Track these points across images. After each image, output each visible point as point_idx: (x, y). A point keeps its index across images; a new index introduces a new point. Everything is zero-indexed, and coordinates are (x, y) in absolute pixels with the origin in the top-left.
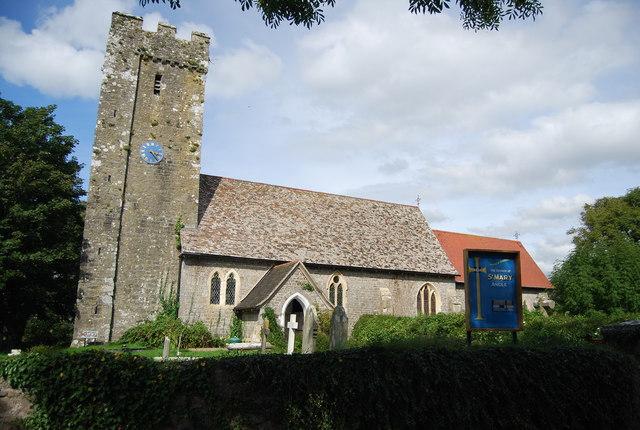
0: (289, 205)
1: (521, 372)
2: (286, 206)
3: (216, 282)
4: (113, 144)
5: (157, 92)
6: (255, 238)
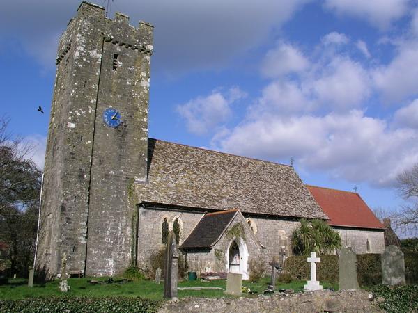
3: (165, 225)
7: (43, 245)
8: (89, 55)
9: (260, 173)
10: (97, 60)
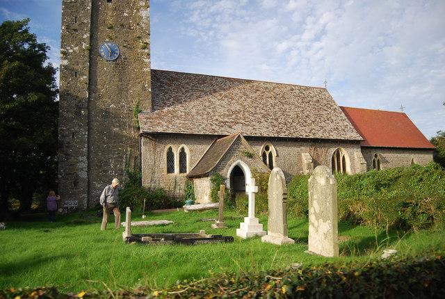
6: (199, 117)
9: (286, 96)
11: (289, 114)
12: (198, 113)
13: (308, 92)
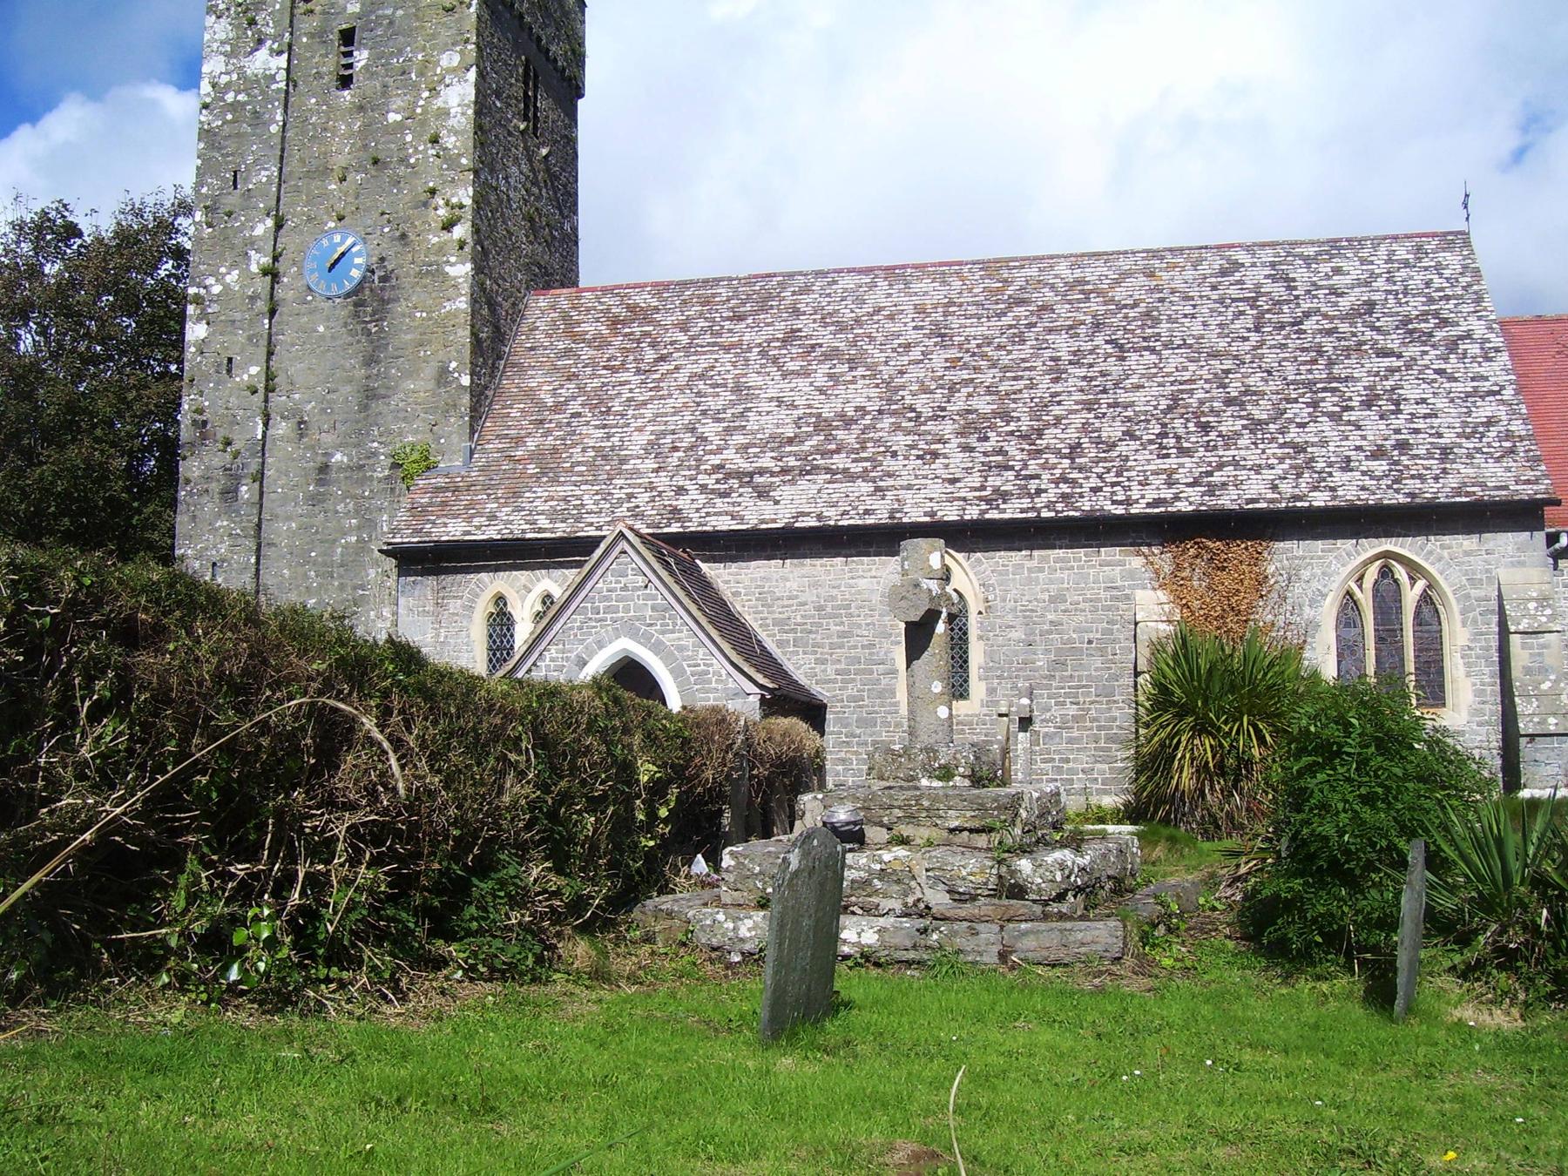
0: (842, 328)
1: (49, 415)
2: (826, 337)
4: (234, 265)
5: (345, 82)
7: (1282, 544)
8: (242, 75)
10: (272, 78)
11: (1123, 397)
12: (652, 448)
13: (1325, 268)
